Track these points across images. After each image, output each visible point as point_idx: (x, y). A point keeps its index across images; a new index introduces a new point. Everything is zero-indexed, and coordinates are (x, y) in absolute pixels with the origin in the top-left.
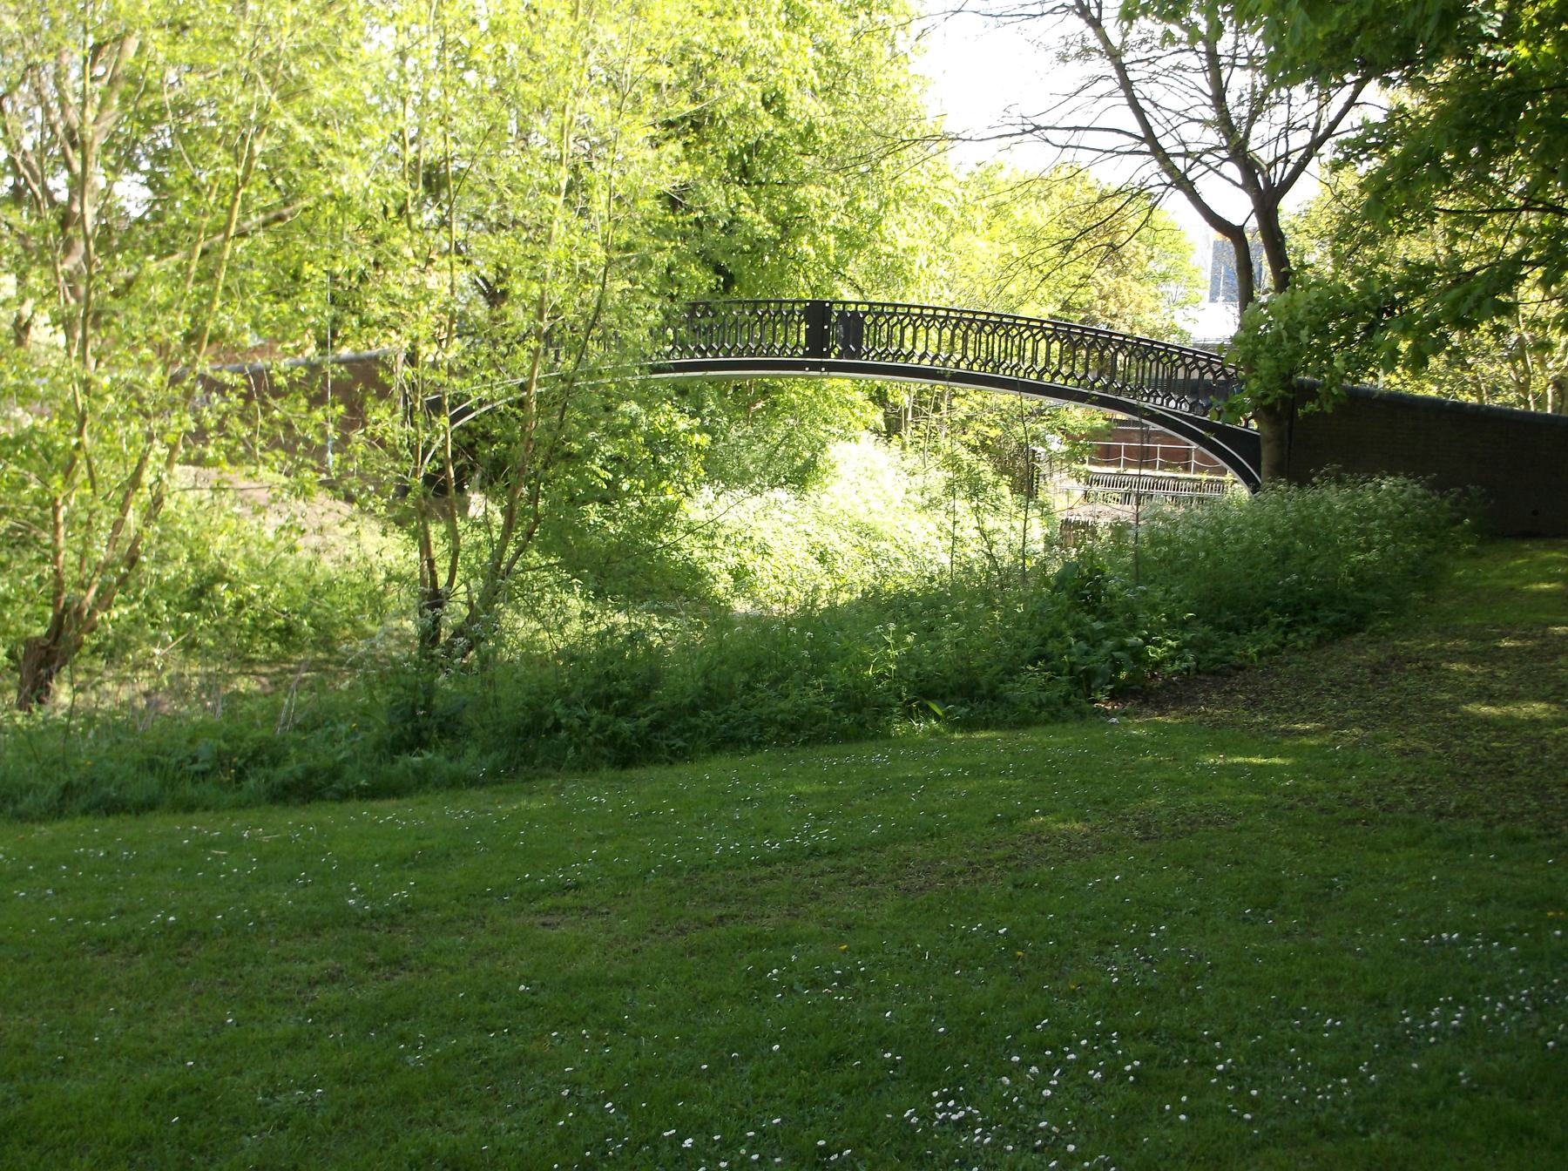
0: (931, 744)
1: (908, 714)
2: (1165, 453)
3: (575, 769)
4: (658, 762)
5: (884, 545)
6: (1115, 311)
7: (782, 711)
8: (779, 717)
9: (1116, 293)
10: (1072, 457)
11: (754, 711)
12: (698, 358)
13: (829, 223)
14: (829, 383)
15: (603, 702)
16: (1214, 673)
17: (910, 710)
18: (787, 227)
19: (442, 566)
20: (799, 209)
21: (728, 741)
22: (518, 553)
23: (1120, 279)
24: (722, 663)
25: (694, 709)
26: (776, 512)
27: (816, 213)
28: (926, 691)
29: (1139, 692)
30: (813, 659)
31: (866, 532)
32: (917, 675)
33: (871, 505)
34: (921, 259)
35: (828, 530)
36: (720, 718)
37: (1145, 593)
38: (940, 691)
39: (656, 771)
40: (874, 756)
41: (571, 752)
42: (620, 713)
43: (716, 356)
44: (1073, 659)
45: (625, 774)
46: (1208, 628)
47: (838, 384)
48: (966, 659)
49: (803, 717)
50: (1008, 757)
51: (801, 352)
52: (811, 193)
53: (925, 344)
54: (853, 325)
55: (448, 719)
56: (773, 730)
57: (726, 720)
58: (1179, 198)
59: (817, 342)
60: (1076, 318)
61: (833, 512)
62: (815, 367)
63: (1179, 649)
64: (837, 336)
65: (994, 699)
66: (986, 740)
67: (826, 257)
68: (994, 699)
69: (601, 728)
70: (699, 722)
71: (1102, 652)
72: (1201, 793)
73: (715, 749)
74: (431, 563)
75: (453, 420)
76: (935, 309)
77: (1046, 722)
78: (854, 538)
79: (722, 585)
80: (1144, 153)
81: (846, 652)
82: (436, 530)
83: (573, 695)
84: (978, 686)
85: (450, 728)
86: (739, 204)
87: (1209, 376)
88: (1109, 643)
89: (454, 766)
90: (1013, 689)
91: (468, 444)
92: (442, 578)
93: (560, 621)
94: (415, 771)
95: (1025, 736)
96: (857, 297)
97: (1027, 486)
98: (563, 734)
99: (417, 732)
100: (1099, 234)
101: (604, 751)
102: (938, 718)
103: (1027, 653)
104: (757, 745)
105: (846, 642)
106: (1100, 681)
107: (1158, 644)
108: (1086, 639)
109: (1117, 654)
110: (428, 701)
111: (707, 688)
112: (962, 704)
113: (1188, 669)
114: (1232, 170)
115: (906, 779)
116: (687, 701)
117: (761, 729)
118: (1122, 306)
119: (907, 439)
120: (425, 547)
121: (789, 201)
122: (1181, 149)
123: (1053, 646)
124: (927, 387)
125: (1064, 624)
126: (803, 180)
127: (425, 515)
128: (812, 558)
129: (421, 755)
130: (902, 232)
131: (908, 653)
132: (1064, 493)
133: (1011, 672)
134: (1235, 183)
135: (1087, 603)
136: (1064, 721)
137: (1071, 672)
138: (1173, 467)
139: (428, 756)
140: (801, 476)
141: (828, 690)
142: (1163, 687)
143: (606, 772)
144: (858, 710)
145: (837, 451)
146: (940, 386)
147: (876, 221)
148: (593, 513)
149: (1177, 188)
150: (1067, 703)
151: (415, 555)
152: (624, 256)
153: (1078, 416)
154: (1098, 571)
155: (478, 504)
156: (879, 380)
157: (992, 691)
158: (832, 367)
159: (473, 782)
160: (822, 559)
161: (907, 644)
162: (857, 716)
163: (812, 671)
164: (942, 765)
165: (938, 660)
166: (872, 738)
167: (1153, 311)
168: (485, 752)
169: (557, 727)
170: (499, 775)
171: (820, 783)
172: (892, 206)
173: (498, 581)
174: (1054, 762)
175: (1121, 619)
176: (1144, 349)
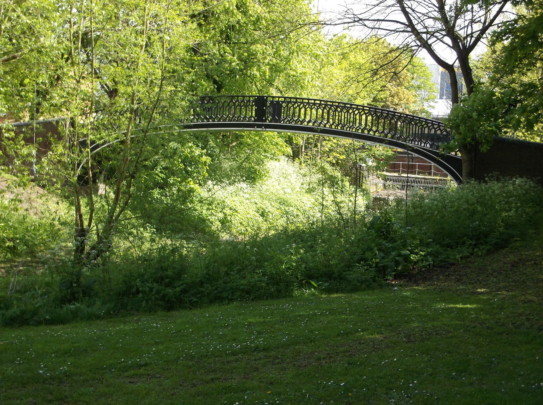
0: (312, 300)
1: (301, 286)
2: (420, 167)
3: (146, 311)
4: (185, 308)
5: (291, 209)
6: (397, 102)
7: (242, 285)
8: (241, 287)
9: (397, 94)
10: (377, 168)
11: (229, 285)
12: (206, 122)
13: (267, 61)
14: (266, 134)
15: (159, 280)
16: (441, 267)
17: (302, 284)
18: (248, 61)
19: (86, 217)
20: (253, 55)
21: (217, 299)
22: (121, 212)
23: (399, 88)
24: (215, 262)
25: (201, 283)
26: (241, 194)
27: (259, 56)
28: (309, 276)
29: (407, 275)
30: (257, 260)
31: (283, 202)
32: (305, 268)
33: (286, 190)
34: (309, 77)
35: (266, 202)
36: (214, 288)
37: (410, 230)
38: (316, 275)
39: (183, 312)
40: (286, 305)
41: (144, 303)
42: (168, 285)
43: (214, 121)
44: (377, 260)
45: (169, 314)
46: (438, 246)
47: (271, 134)
48: (328, 260)
49: (252, 287)
50: (347, 305)
51: (253, 119)
52: (258, 47)
53: (309, 116)
54: (277, 106)
55: (87, 288)
56: (238, 293)
57: (216, 289)
58: (423, 53)
59: (260, 115)
60: (380, 105)
61: (268, 193)
62: (259, 126)
63: (425, 256)
64: (270, 113)
65: (341, 279)
66: (337, 298)
67: (265, 76)
68: (341, 279)
69: (158, 292)
70: (204, 289)
71: (391, 257)
72: (434, 321)
73: (212, 302)
74: (81, 216)
75: (92, 150)
76: (315, 100)
77: (364, 290)
78: (277, 205)
79: (216, 225)
80: (408, 32)
81: (272, 257)
82: (83, 202)
83: (146, 277)
84: (333, 273)
85: (88, 292)
86: (225, 52)
87: (439, 132)
88: (394, 253)
89: (90, 310)
90: (349, 274)
91: (98, 159)
92: (86, 223)
93: (139, 242)
94: (72, 312)
95: (355, 296)
96: (279, 95)
97: (357, 181)
98: (140, 295)
99: (73, 294)
100: (389, 66)
101: (160, 302)
102: (314, 288)
103: (356, 258)
104: (231, 300)
105: (272, 252)
106: (390, 270)
107: (416, 254)
108: (383, 251)
109: (397, 258)
110: (78, 279)
111: (207, 274)
112: (326, 282)
113: (429, 265)
114: (447, 40)
115: (299, 316)
116: (198, 280)
117: (233, 293)
118: (400, 100)
119: (302, 160)
120: (78, 210)
121: (248, 51)
122: (425, 30)
123: (368, 254)
124: (312, 136)
125: (373, 245)
126: (255, 42)
127: (78, 193)
128: (257, 215)
129: (74, 304)
130: (300, 66)
131: (301, 258)
132: (375, 185)
133: (349, 266)
134: (449, 46)
135: (384, 235)
136: (373, 289)
137: (376, 267)
138: (424, 173)
139: (78, 305)
140: (252, 176)
141: (264, 275)
142: (418, 273)
143: (160, 313)
144: (278, 284)
145: (270, 164)
146: (317, 135)
147: (288, 60)
148: (156, 193)
149: (423, 47)
150: (374, 281)
151: (73, 212)
152: (171, 76)
153: (380, 150)
154: (389, 220)
155: (102, 188)
156: (289, 133)
157: (339, 275)
158: (267, 126)
159: (98, 317)
160: (262, 215)
161: (301, 254)
162: (279, 287)
163: (257, 266)
164: (316, 309)
165: (315, 261)
166: (284, 297)
167: (414, 102)
168: (104, 303)
169: (138, 292)
170: (110, 314)
171: (260, 317)
172: (295, 54)
173: (111, 225)
174: (368, 307)
175: (399, 242)
176: (411, 120)
